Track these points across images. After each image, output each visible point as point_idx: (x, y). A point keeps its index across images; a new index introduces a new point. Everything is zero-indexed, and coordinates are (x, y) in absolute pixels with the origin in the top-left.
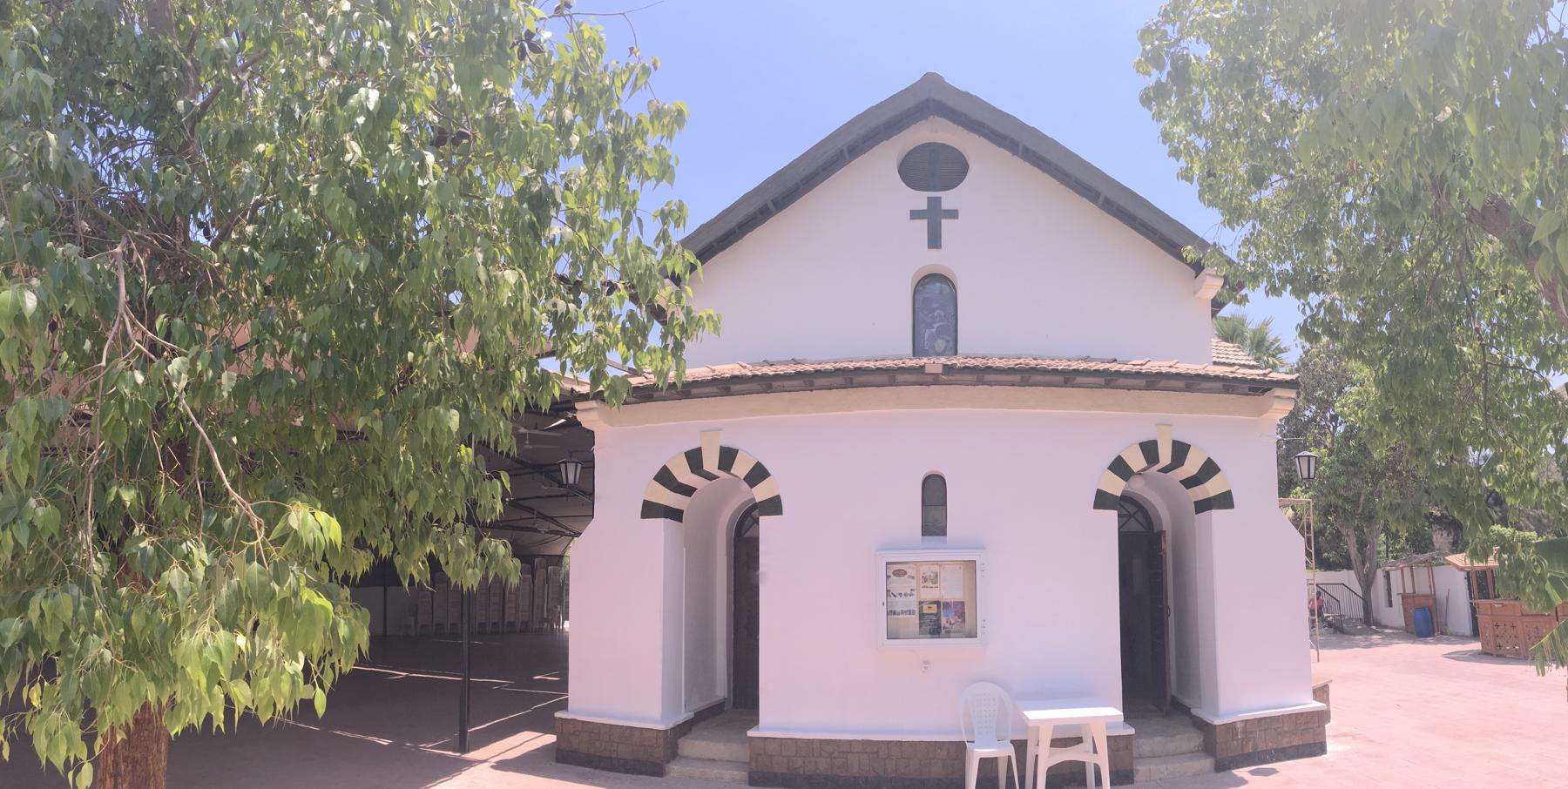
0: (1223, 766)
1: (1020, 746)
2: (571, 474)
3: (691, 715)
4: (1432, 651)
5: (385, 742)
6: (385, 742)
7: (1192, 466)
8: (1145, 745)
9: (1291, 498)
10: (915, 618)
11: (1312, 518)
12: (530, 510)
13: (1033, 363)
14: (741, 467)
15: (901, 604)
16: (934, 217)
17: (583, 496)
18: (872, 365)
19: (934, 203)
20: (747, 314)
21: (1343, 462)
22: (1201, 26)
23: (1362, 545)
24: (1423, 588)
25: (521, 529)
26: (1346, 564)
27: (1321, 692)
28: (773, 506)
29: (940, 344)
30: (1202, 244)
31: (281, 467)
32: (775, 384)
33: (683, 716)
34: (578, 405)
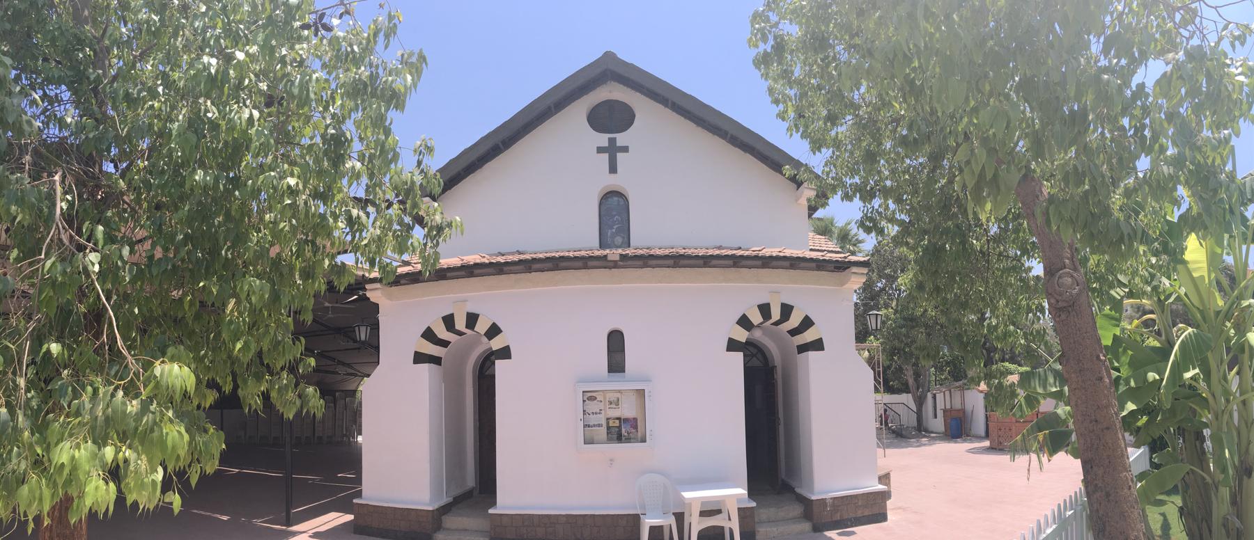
0: (818, 528)
1: (680, 517)
2: (363, 334)
3: (451, 499)
4: (959, 448)
5: (225, 518)
6: (225, 518)
7: (795, 321)
8: (764, 514)
9: (867, 344)
10: (604, 430)
11: (881, 357)
12: (334, 359)
13: (682, 252)
14: (482, 327)
15: (593, 420)
16: (612, 151)
17: (372, 348)
18: (571, 254)
19: (612, 141)
20: (481, 222)
21: (905, 319)
22: (793, 12)
23: (917, 375)
24: (957, 405)
25: (327, 372)
26: (904, 389)
27: (884, 479)
28: (505, 353)
29: (619, 240)
30: (797, 164)
31: (162, 329)
32: (505, 269)
33: (445, 500)
34: (367, 286)
